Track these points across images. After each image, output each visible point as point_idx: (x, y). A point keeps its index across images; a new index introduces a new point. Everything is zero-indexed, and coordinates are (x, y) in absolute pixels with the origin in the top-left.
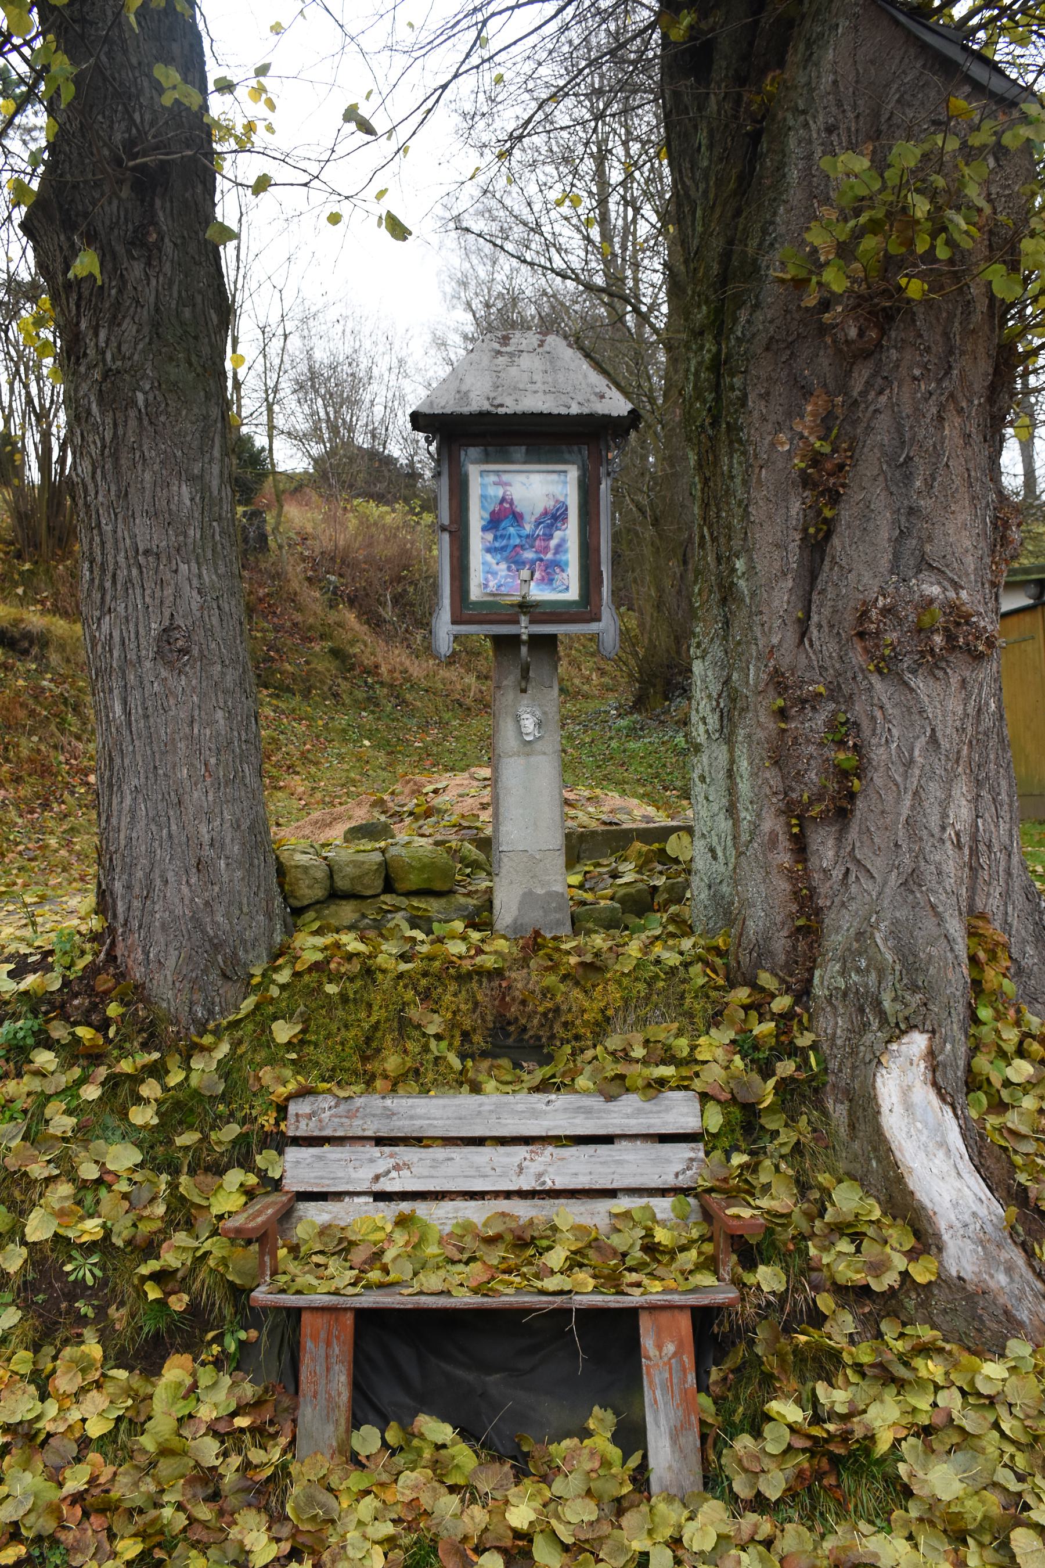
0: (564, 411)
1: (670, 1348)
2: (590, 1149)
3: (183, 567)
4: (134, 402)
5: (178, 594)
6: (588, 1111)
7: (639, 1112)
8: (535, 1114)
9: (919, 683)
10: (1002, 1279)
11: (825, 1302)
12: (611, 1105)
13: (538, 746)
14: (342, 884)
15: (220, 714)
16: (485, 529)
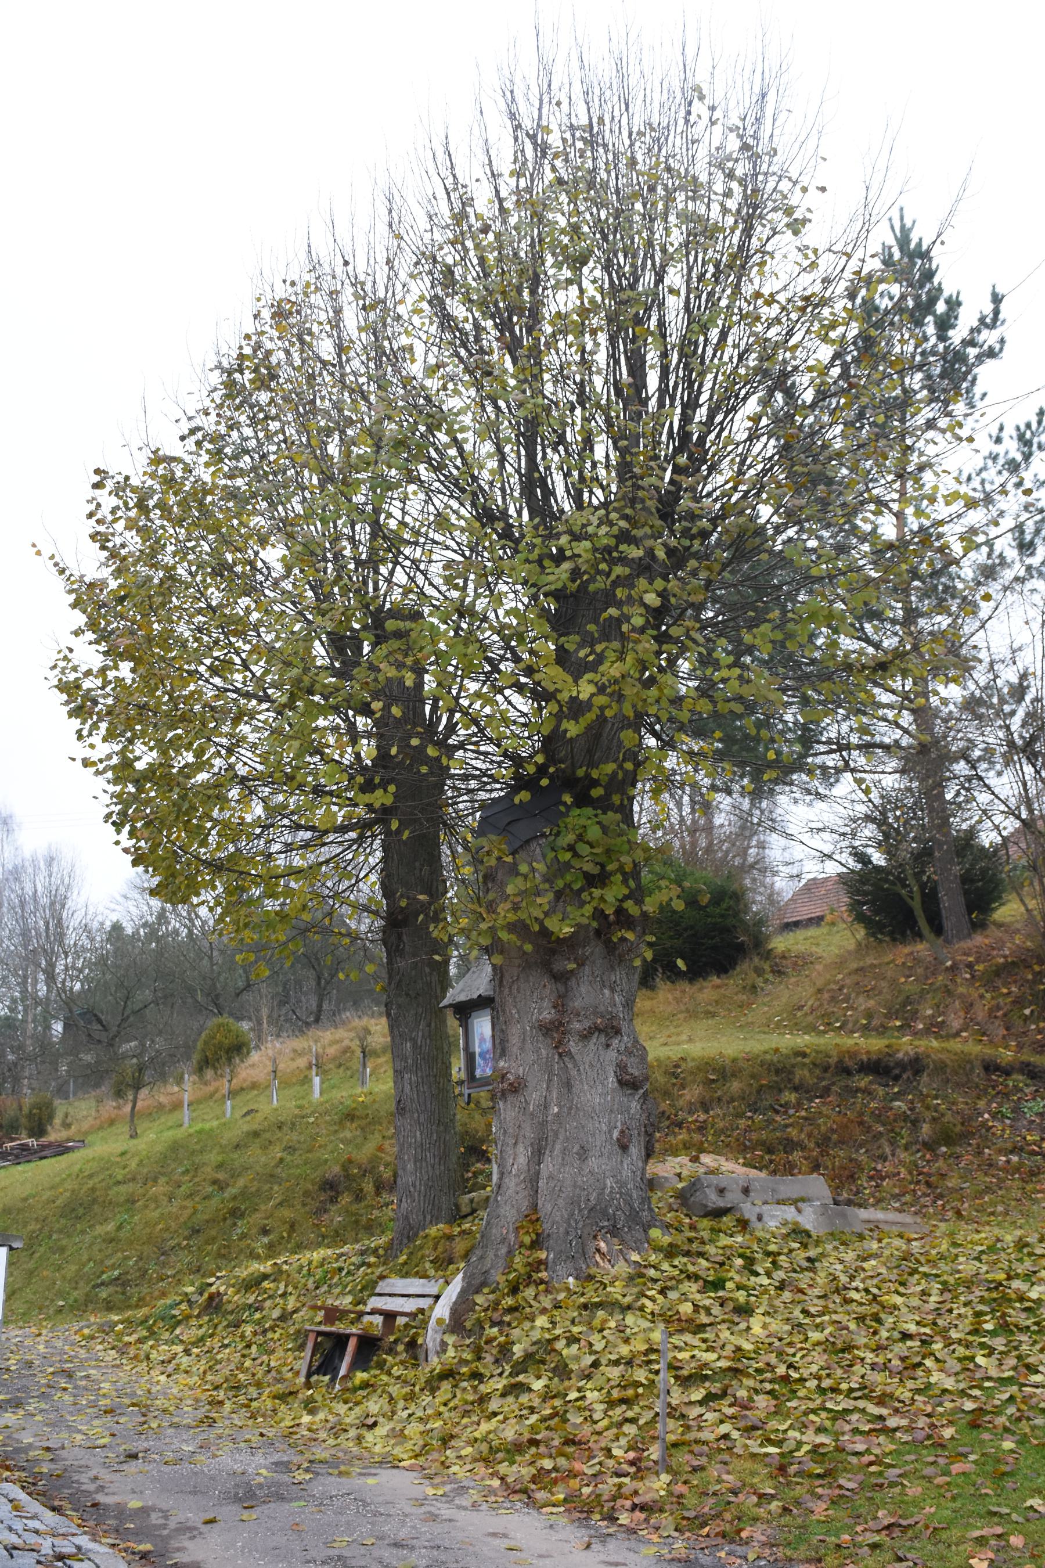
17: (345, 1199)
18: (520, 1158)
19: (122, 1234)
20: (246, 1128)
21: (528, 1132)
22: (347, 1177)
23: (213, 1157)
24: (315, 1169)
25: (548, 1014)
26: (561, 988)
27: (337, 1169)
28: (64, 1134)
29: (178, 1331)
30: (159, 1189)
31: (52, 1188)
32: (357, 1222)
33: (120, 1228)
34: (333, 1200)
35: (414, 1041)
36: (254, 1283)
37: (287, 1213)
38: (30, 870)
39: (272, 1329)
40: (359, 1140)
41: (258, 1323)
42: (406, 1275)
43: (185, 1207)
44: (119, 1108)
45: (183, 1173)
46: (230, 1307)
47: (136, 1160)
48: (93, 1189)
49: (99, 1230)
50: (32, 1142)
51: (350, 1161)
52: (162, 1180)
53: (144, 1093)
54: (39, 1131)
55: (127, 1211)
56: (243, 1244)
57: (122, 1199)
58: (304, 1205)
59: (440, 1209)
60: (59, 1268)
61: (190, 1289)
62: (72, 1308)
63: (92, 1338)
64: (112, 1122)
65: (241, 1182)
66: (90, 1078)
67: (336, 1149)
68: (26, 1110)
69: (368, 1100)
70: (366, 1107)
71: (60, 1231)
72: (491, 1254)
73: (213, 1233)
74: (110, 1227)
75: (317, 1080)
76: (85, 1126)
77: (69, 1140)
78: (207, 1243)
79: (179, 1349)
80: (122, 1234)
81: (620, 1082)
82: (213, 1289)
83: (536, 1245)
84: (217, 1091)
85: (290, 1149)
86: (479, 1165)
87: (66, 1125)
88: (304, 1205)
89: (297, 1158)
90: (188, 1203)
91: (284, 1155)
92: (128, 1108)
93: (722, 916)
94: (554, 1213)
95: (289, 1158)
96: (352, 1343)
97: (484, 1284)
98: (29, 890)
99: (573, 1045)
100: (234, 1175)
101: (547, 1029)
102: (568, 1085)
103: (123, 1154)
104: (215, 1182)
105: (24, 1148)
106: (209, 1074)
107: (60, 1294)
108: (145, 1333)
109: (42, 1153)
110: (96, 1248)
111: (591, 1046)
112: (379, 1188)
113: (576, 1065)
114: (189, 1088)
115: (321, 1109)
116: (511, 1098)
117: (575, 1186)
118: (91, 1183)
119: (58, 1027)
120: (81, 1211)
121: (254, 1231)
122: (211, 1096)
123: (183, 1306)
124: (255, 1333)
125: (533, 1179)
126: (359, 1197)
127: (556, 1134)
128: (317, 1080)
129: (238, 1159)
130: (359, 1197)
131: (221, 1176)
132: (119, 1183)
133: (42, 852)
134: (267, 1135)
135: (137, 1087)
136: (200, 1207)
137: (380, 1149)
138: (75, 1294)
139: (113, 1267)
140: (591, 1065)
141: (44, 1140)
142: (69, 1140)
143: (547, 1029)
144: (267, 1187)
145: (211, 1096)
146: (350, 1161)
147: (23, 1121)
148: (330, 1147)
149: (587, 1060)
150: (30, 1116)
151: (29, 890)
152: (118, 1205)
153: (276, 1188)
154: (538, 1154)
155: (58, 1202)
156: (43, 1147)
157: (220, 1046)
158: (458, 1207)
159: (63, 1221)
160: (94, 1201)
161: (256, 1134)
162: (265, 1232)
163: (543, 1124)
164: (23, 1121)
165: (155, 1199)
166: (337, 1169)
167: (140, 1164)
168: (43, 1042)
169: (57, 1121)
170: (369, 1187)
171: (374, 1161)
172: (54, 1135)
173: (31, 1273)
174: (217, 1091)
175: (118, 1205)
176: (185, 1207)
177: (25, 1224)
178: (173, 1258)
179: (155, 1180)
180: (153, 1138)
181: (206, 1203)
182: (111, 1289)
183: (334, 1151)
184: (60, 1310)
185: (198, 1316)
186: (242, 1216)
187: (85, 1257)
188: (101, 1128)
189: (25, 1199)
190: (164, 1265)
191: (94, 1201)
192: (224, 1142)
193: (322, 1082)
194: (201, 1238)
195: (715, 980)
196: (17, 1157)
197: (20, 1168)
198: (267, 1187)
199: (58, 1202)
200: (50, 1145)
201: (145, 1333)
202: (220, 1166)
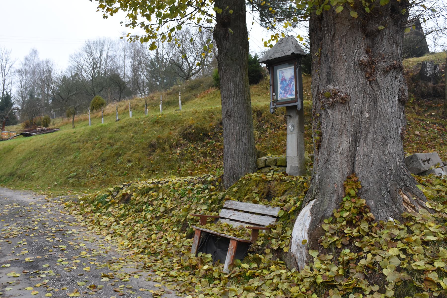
0: (280, 56)
1: (232, 247)
2: (259, 216)
3: (231, 99)
4: (222, 69)
5: (229, 105)
6: (262, 209)
7: (270, 210)
8: (255, 208)
9: (329, 111)
10: (298, 255)
11: (267, 251)
12: (266, 208)
13: (293, 132)
14: (267, 163)
15: (237, 127)
16: (280, 84)
17: (158, 151)
18: (345, 144)
19: (76, 160)
20: (118, 125)
21: (350, 128)
22: (159, 143)
23: (107, 135)
24: (146, 140)
25: (364, 58)
26: (369, 42)
27: (155, 140)
28: (53, 127)
29: (110, 209)
30: (89, 145)
31: (50, 143)
32: (164, 159)
33: (75, 158)
34: (154, 151)
35: (234, 82)
36: (145, 192)
37: (136, 155)
38: (42, 64)
39: (161, 217)
40: (161, 130)
41: (152, 212)
42: (240, 200)
43: (99, 152)
44: (68, 120)
45: (97, 140)
46: (136, 202)
47: (80, 135)
48: (65, 144)
49: (68, 158)
50: (44, 128)
51: (159, 137)
52: (89, 142)
53: (76, 116)
54: (46, 126)
55: (77, 152)
56: (121, 165)
57: (75, 148)
58: (143, 152)
59: (249, 165)
60: (55, 171)
61: (112, 189)
62: (60, 185)
63: (70, 206)
64: (67, 124)
65: (119, 144)
66: (60, 114)
67: (153, 133)
68: (42, 120)
69: (162, 117)
70: (162, 119)
71: (54, 158)
72: (327, 199)
73: (110, 161)
74: (72, 157)
75: (131, 112)
76: (59, 124)
77: (55, 128)
78: (108, 164)
79: (112, 219)
80: (76, 160)
81: (399, 100)
82: (124, 191)
83: (358, 195)
84: (97, 116)
85: (136, 133)
86: (207, 140)
87: (54, 124)
88: (143, 152)
89: (139, 136)
90: (99, 150)
91: (134, 135)
92: (72, 120)
93: (256, 67)
94: (367, 175)
95: (136, 136)
96: (232, 246)
97: (323, 217)
98: (42, 69)
99: (379, 77)
100: (116, 141)
101: (363, 66)
102: (375, 101)
103: (74, 133)
104: (109, 143)
105: (42, 130)
106: (95, 111)
107: (55, 180)
108: (94, 208)
109: (47, 131)
110: (67, 164)
111: (389, 77)
112: (171, 147)
113: (379, 89)
114: (89, 115)
115: (145, 119)
116: (339, 108)
117: (381, 160)
118: (64, 142)
119: (50, 101)
120: (61, 151)
121: (125, 161)
122: (96, 117)
123: (110, 197)
124: (152, 218)
125: (352, 158)
126: (163, 150)
127: (368, 131)
128: (131, 112)
129: (117, 136)
130: (163, 150)
131: (111, 141)
132: (74, 142)
133: (45, 60)
134: (127, 128)
135: (75, 114)
136: (104, 152)
137: (170, 133)
138: (61, 180)
139: (74, 172)
140: (388, 89)
141: (48, 128)
142: (55, 128)
143: (363, 66)
144: (129, 146)
145: (96, 117)
146: (159, 137)
147: (42, 123)
148: (151, 132)
149: (385, 86)
150: (44, 122)
151: (42, 69)
152: (74, 150)
153: (132, 146)
154: (355, 142)
155: (53, 148)
156: (47, 130)
157: (97, 104)
158: (257, 163)
159: (55, 154)
160: (65, 148)
161: (122, 127)
162: (129, 161)
163: (360, 123)
164: (42, 123)
165: (87, 148)
166: (155, 140)
167: (81, 136)
168: (47, 104)
169: (51, 123)
170: (167, 147)
171: (168, 138)
172: (51, 127)
173: (45, 172)
174: (97, 116)
175: (74, 150)
176: (99, 152)
177: (42, 155)
178: (95, 170)
179: (87, 142)
180: (82, 129)
181: (106, 150)
182: (74, 179)
183: (154, 134)
184: (55, 186)
185: (118, 203)
186: (120, 155)
187: (64, 167)
188: (63, 125)
189: (42, 146)
190: (92, 172)
191: (65, 148)
192: (111, 130)
193: (132, 113)
194: (105, 163)
195: (255, 86)
196: (40, 132)
197: (40, 136)
198: (129, 146)
199: (53, 148)
200: (49, 129)
201: (94, 208)
202: (110, 138)
